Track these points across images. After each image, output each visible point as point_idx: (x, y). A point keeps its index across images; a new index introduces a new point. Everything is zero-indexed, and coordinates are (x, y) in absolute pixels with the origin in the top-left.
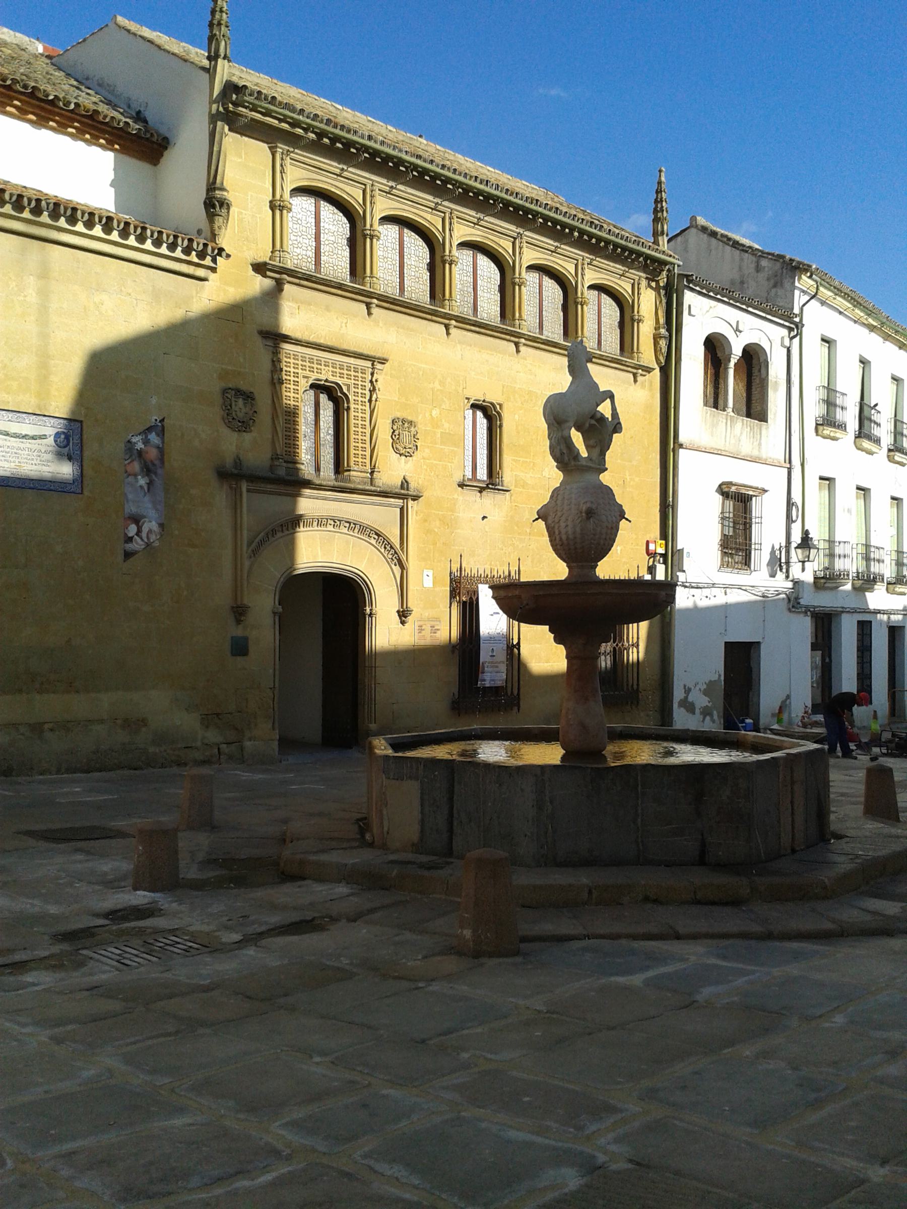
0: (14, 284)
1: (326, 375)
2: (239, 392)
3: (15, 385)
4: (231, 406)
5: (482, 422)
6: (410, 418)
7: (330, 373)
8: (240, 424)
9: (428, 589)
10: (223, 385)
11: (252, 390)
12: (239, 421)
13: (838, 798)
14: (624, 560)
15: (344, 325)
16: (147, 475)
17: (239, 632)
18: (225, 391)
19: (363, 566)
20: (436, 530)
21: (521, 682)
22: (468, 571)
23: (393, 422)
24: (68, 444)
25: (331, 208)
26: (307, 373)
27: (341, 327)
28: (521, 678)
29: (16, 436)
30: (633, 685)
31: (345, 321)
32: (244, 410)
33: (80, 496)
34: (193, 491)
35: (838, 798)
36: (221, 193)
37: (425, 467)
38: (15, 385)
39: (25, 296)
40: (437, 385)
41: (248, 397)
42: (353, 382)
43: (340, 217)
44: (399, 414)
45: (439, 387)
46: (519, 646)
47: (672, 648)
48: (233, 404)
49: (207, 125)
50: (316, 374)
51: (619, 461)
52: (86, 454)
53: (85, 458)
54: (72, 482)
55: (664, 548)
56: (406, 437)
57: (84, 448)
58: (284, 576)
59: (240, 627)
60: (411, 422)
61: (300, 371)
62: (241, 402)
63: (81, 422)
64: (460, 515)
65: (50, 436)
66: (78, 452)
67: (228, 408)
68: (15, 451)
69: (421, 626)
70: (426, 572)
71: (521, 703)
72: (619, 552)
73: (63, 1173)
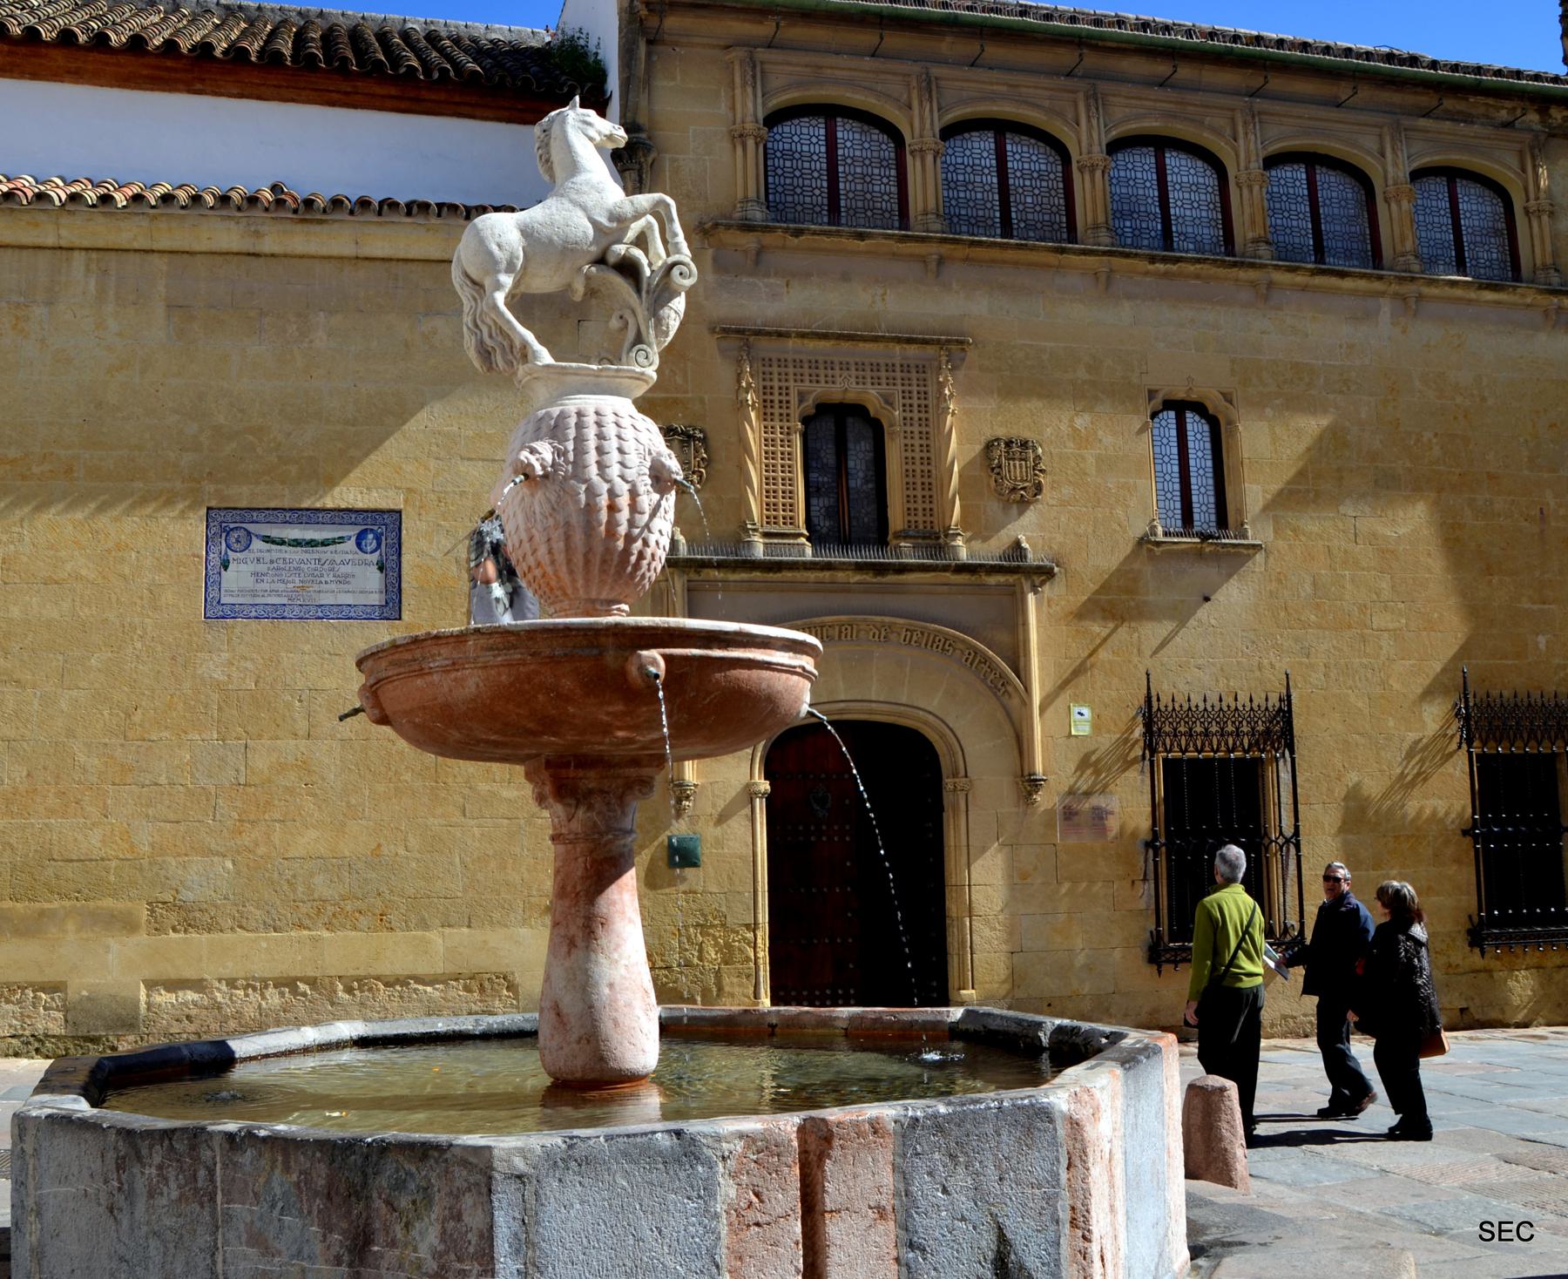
0: (295, 327)
1: (843, 388)
3: (293, 470)
5: (1196, 427)
9: (1411, 924)
14: (1556, 661)
15: (878, 298)
16: (510, 580)
19: (935, 703)
22: (1165, 699)
24: (379, 545)
26: (806, 386)
27: (874, 302)
29: (297, 543)
31: (880, 291)
38: (293, 470)
39: (311, 342)
40: (1082, 374)
44: (1001, 432)
45: (1087, 377)
49: (1336, 1146)
51: (1526, 472)
52: (407, 558)
53: (404, 565)
56: (1016, 471)
57: (404, 550)
60: (1024, 444)
63: (400, 512)
64: (1151, 598)
65: (350, 538)
66: (395, 557)
68: (296, 565)
70: (1075, 710)
72: (1542, 646)
73: (732, 1193)
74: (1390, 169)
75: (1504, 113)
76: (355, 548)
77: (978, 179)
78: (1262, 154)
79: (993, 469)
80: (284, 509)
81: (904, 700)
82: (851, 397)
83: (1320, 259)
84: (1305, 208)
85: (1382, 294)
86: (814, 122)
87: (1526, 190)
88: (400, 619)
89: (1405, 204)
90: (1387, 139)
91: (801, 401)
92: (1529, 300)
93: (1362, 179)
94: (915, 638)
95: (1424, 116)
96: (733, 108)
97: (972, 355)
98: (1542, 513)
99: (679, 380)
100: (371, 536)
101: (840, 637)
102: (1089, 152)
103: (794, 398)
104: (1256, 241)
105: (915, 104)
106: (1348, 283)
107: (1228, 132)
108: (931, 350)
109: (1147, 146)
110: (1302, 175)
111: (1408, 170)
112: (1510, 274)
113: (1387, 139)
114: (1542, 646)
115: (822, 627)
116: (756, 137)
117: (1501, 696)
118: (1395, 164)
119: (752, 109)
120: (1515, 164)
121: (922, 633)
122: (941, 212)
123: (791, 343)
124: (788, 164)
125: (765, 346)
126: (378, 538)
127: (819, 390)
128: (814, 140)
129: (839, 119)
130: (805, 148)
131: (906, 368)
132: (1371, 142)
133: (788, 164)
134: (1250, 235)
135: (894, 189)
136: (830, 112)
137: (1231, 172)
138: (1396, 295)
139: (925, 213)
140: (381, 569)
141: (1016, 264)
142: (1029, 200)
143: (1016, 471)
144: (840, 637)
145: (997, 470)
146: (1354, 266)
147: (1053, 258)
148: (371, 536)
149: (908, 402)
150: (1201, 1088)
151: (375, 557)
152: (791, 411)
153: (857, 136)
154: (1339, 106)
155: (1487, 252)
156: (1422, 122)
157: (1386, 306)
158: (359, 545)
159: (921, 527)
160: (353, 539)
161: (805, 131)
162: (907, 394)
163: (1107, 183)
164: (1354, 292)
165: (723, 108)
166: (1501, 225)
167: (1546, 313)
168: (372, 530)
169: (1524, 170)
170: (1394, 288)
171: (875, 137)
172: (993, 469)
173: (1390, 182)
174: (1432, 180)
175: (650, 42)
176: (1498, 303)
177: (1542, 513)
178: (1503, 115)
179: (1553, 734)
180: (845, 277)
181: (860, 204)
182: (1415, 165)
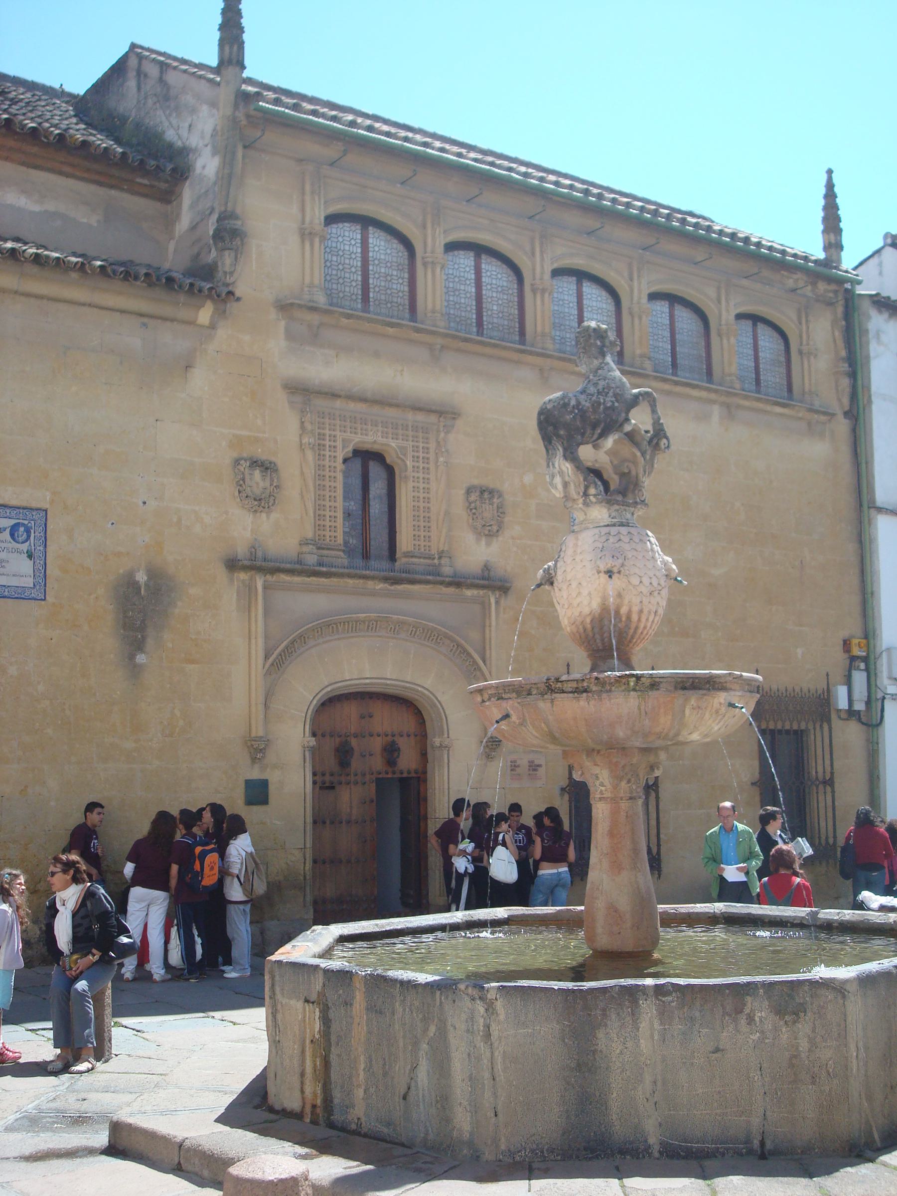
1: (372, 439)
2: (255, 463)
4: (243, 480)
6: (491, 486)
7: (380, 434)
8: (256, 503)
10: (235, 455)
11: (273, 459)
12: (255, 500)
13: (196, 70)
17: (255, 774)
18: (237, 462)
20: (533, 632)
21: (662, 836)
23: (469, 491)
24: (29, 537)
25: (383, 235)
26: (348, 435)
28: (662, 831)
30: (827, 838)
32: (261, 484)
33: (43, 602)
34: (193, 591)
35: (196, 70)
36: (232, 222)
37: (515, 549)
41: (267, 467)
42: (411, 443)
43: (396, 245)
44: (476, 482)
46: (657, 787)
47: (882, 806)
48: (247, 477)
50: (359, 436)
52: (52, 548)
54: (32, 586)
55: (865, 649)
56: (488, 512)
58: (317, 698)
59: (257, 766)
60: (491, 492)
61: (338, 433)
62: (257, 473)
66: (42, 548)
67: (241, 484)
69: (515, 762)
71: (663, 865)
72: (799, 656)
74: (724, 313)
75: (791, 281)
76: (9, 538)
77: (462, 287)
78: (648, 292)
79: (471, 510)
80: (31, 509)
81: (408, 679)
82: (376, 448)
83: (675, 374)
84: (667, 334)
85: (714, 402)
86: (353, 228)
87: (801, 337)
88: (45, 600)
89: (733, 340)
90: (723, 291)
91: (344, 448)
92: (800, 415)
93: (703, 318)
94: (418, 633)
95: (746, 278)
96: (303, 210)
97: (459, 423)
98: (802, 563)
99: (259, 422)
100: (22, 529)
101: (368, 628)
102: (541, 279)
103: (339, 444)
104: (641, 356)
105: (429, 225)
106: (695, 393)
107: (626, 274)
108: (433, 418)
109: (572, 276)
110: (666, 309)
111: (550, 270)
112: (705, 378)
113: (723, 291)
114: (799, 656)
115: (356, 622)
116: (320, 237)
117: (794, 690)
118: (728, 311)
119: (317, 213)
120: (794, 317)
121: (423, 630)
122: (323, 286)
123: (338, 403)
124: (334, 258)
125: (321, 403)
126: (28, 531)
127: (357, 440)
128: (353, 242)
129: (370, 228)
130: (347, 248)
131: (415, 429)
132: (712, 292)
133: (334, 258)
134: (638, 352)
135: (406, 289)
136: (366, 222)
137: (625, 304)
138: (723, 404)
139: (433, 312)
140: (30, 556)
141: (490, 357)
142: (495, 308)
143: (488, 512)
144: (368, 628)
145: (474, 511)
146: (694, 379)
147: (515, 356)
148: (22, 529)
149: (416, 454)
150: (328, 970)
151: (25, 547)
152: (337, 454)
153: (383, 243)
154: (696, 264)
155: (772, 377)
156: (745, 282)
157: (716, 410)
158: (12, 535)
159: (422, 550)
160: (8, 531)
161: (347, 234)
162: (416, 449)
163: (323, 251)
164: (699, 399)
165: (295, 209)
166: (783, 359)
167: (809, 424)
168: (23, 525)
169: (800, 323)
170: (723, 399)
171: (395, 246)
172: (471, 510)
173: (723, 322)
174: (565, 278)
175: (245, 147)
176: (781, 415)
177: (802, 563)
178: (790, 283)
179: (767, 716)
180: (377, 354)
181: (383, 297)
182: (555, 266)
